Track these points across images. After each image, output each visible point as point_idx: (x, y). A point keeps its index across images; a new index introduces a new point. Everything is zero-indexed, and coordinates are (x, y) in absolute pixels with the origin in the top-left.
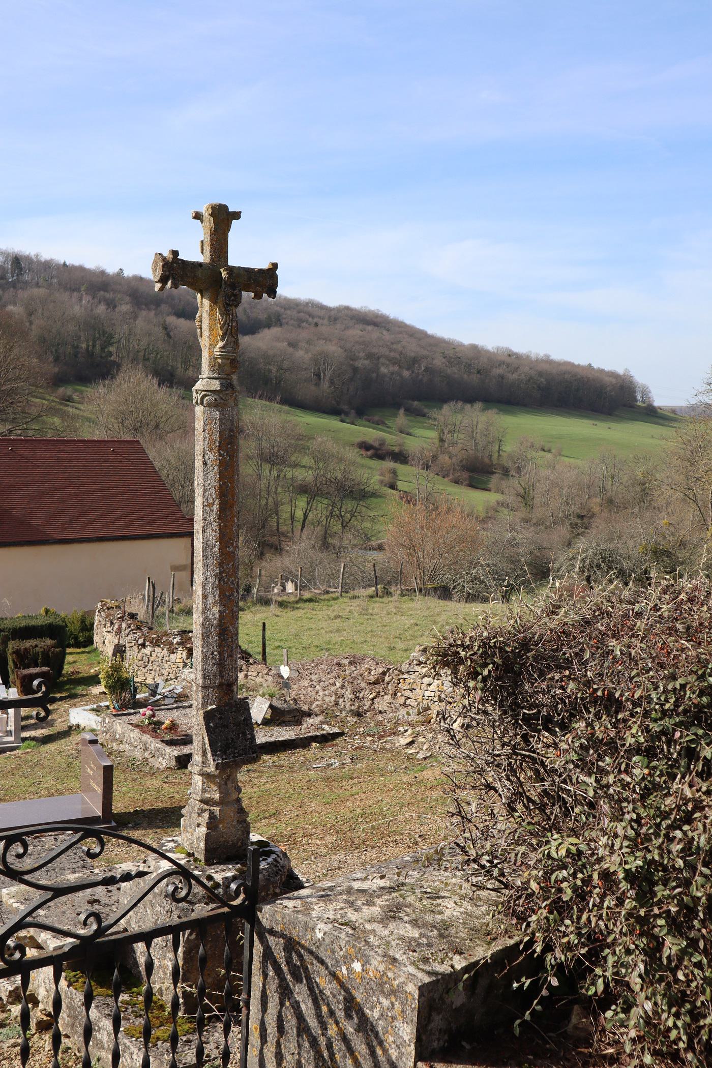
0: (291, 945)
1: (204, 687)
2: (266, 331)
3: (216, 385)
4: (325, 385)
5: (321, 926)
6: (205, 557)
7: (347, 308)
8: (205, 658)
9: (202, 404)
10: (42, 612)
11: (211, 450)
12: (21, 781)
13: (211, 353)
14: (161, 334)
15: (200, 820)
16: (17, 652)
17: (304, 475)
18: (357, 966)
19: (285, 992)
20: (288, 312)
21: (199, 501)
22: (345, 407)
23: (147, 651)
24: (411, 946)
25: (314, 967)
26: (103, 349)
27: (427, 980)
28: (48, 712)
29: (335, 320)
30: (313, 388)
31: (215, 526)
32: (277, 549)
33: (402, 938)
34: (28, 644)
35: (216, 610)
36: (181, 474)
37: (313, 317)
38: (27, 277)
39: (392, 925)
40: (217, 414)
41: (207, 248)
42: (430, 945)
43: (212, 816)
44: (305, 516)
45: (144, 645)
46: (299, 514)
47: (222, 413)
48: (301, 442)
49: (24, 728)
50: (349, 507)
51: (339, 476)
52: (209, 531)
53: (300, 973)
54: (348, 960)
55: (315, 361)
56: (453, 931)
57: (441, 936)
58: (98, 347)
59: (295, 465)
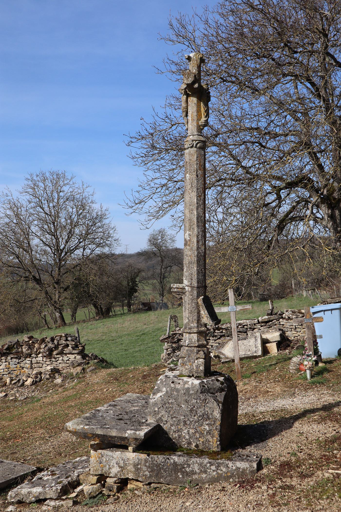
1: (198, 287)
9: (196, 147)
11: (200, 170)
41: (219, 447)
52: (200, 209)
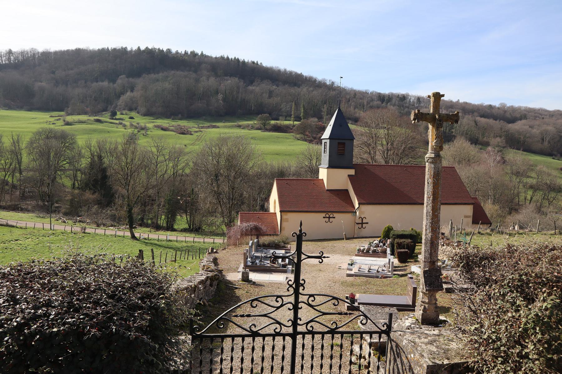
0: (397, 346)
2: (519, 121)
3: (433, 156)
4: (546, 143)
5: (405, 341)
6: (427, 216)
7: (559, 111)
8: (425, 252)
10: (411, 229)
12: (390, 289)
13: (432, 144)
14: (473, 124)
15: (420, 308)
16: (398, 243)
17: (530, 181)
18: (412, 355)
19: (395, 361)
20: (530, 113)
21: (426, 196)
22: (555, 153)
23: (445, 247)
24: (431, 353)
25: (402, 354)
26: (449, 130)
27: (431, 364)
28: (322, 260)
29: (553, 116)
30: (540, 145)
31: (431, 205)
32: (516, 210)
33: (429, 350)
34: (402, 240)
35: (430, 235)
36: (477, 180)
37: (542, 115)
38: (422, 105)
39: (428, 346)
40: (433, 166)
42: (438, 354)
43: (425, 308)
44: (531, 198)
45: (443, 245)
46: (529, 197)
47: (435, 165)
48: (531, 167)
49: (395, 271)
50: (553, 196)
51: (548, 182)
52: (429, 207)
53: (399, 355)
54: (410, 353)
55: (542, 133)
56: (450, 352)
57: (444, 353)
58: (448, 130)
59: (529, 177)
